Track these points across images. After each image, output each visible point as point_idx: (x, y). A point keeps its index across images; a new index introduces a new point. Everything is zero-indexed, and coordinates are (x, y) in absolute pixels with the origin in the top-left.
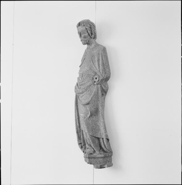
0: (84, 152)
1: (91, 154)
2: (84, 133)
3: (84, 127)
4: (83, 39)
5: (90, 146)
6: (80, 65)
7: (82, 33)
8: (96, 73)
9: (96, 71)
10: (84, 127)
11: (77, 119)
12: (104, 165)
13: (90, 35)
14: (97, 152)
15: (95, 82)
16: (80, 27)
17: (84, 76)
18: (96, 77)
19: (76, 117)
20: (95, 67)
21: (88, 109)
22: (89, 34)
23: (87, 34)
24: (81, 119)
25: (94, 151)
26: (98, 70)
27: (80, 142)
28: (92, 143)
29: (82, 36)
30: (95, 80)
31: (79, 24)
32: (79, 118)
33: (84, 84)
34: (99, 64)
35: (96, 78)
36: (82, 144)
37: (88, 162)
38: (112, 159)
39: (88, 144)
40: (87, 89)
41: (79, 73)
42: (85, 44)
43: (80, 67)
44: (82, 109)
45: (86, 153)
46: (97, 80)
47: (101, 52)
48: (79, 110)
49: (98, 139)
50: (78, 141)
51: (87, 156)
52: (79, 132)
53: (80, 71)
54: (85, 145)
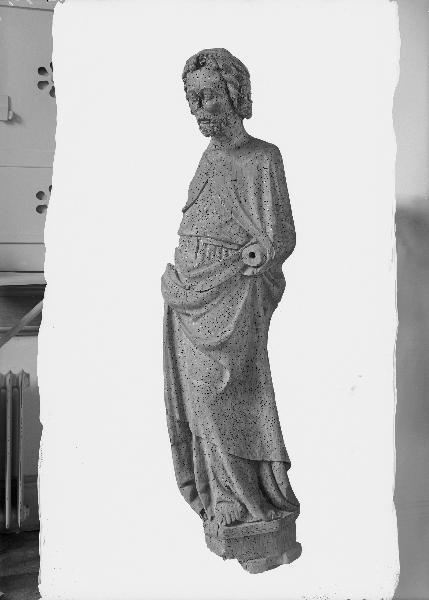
0: (202, 513)
1: (237, 522)
2: (206, 450)
3: (202, 423)
4: (207, 115)
5: (229, 491)
6: (184, 205)
7: (207, 95)
8: (249, 236)
9: (252, 230)
10: (202, 423)
11: (174, 395)
12: (277, 558)
13: (236, 103)
14: (255, 514)
15: (246, 267)
16: (201, 74)
17: (206, 244)
18: (252, 249)
19: (168, 389)
20: (249, 216)
21: (224, 362)
22: (231, 102)
23: (223, 100)
24: (189, 395)
25: (245, 512)
26: (259, 225)
27: (185, 479)
28: (234, 480)
29: (207, 104)
30: (247, 261)
31: (198, 62)
32: (180, 391)
33: (210, 274)
34: (260, 208)
35: (252, 255)
36: (194, 485)
37: (223, 551)
38: (37, 558)
39: (219, 485)
40: (218, 293)
41: (180, 233)
42: (208, 136)
43: (184, 211)
44: (194, 362)
45: (212, 518)
46: (257, 260)
47: (267, 166)
48: (181, 361)
49: (257, 465)
50: (178, 473)
51: (221, 533)
52: (183, 438)
53: (183, 226)
54: (207, 489)
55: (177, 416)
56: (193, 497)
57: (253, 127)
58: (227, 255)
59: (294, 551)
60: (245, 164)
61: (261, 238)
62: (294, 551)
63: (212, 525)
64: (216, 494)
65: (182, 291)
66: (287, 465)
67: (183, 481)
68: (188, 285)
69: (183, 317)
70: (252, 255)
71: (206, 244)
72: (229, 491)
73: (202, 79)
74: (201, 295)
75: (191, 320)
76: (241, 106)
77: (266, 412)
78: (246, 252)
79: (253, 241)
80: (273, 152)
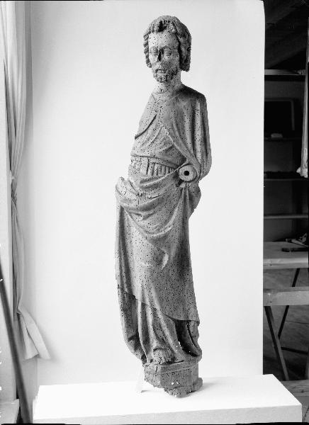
0: (144, 358)
7: (196, 324)
8: (184, 159)
26: (192, 152)
36: (137, 340)
39: (158, 338)
54: (147, 341)
55: (126, 290)
56: (137, 347)
57: (187, 79)
58: (169, 172)
59: (266, 371)
60: (184, 104)
61: (193, 161)
62: (266, 371)
63: (152, 366)
64: (154, 343)
65: (134, 197)
66: (198, 323)
67: (130, 336)
68: (142, 192)
69: (135, 216)
70: (187, 173)
71: (154, 163)
72: (163, 341)
73: (158, 40)
74: (151, 201)
75: (142, 218)
76: (184, 64)
77: (192, 310)
78: (182, 171)
79: (187, 162)
80: (201, 98)
